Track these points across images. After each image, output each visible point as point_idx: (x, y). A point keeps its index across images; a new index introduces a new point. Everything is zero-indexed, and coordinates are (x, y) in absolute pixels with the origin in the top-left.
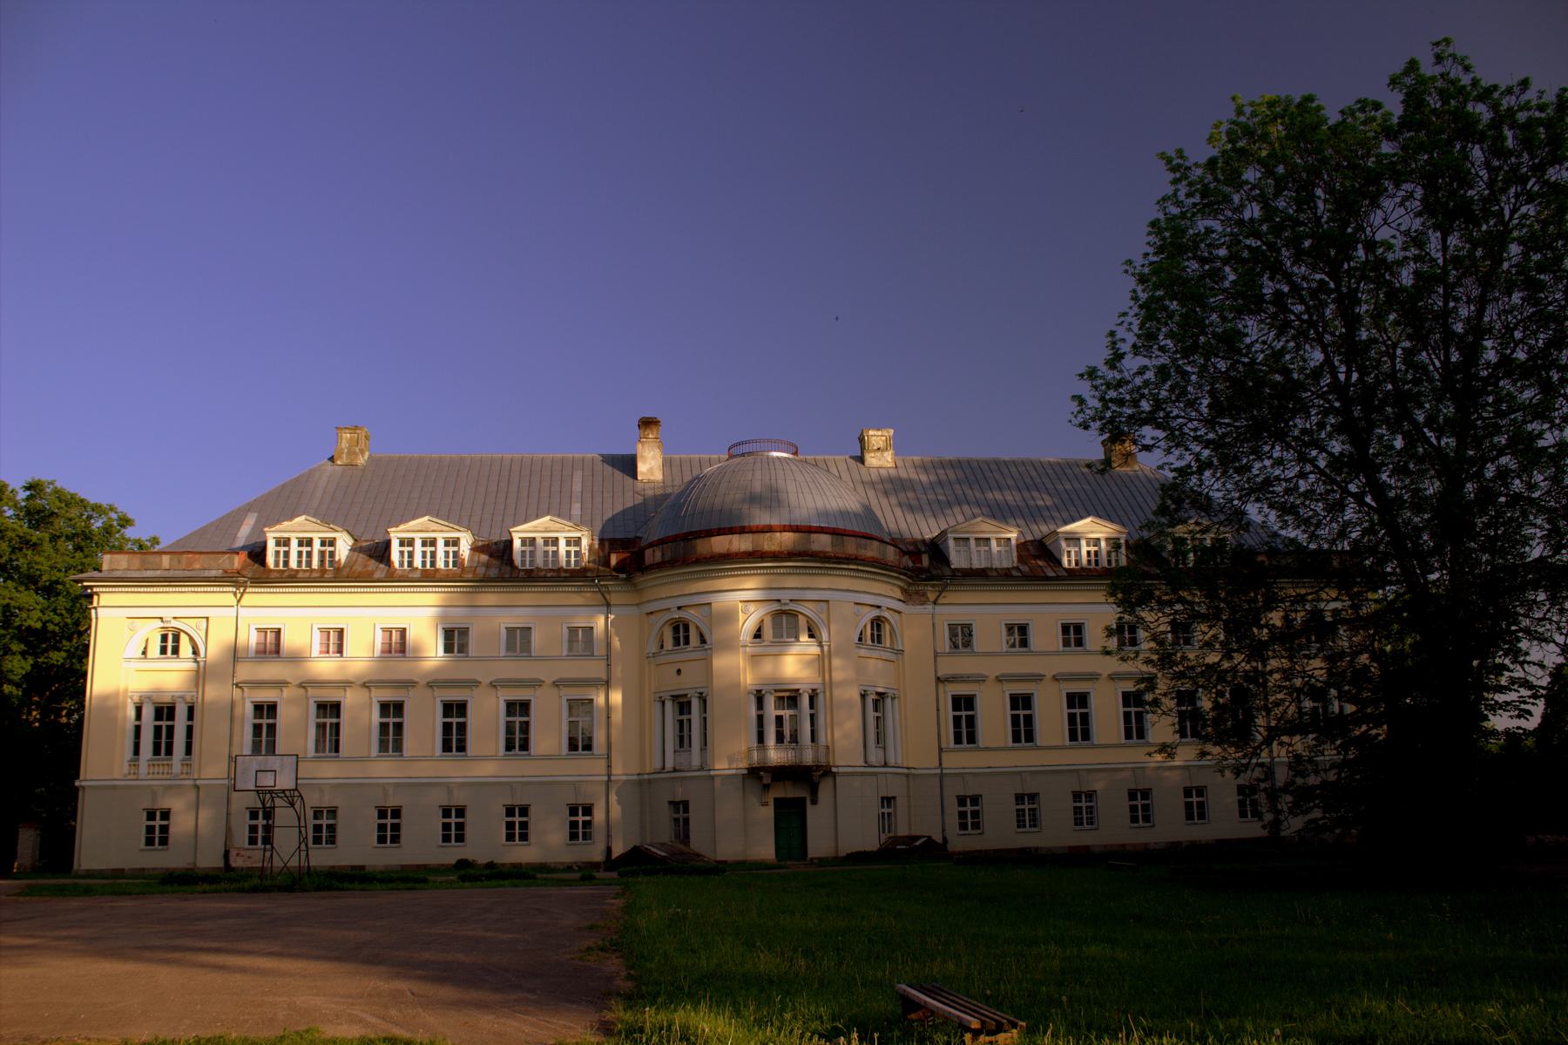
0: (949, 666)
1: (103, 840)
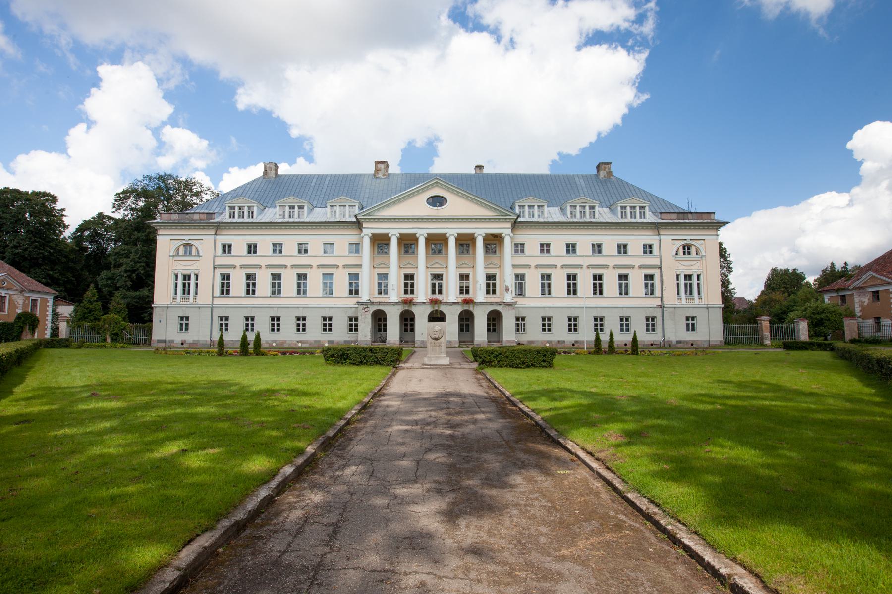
0: (219, 262)
1: (164, 328)
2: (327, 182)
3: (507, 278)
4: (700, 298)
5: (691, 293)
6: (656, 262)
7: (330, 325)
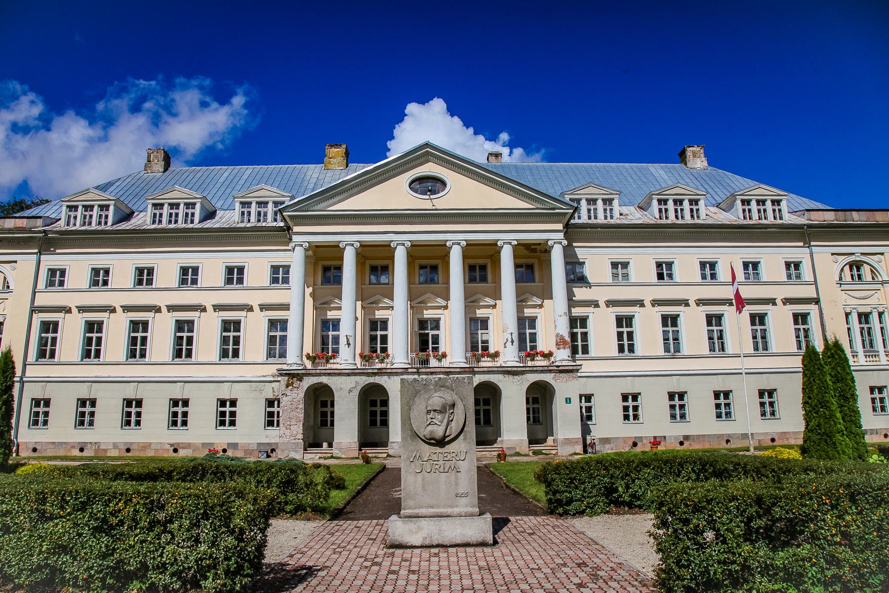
0: (44, 299)
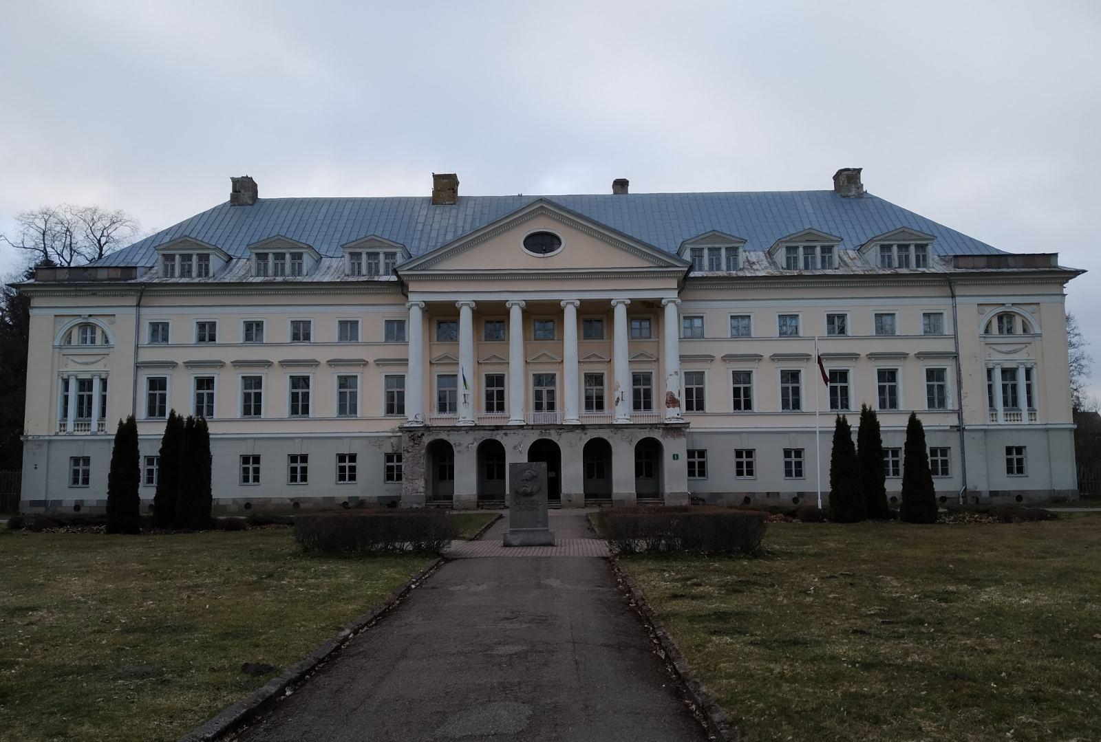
0: (148, 355)
2: (346, 213)
3: (672, 382)
4: (1032, 412)
5: (1015, 402)
6: (948, 346)
7: (353, 469)
